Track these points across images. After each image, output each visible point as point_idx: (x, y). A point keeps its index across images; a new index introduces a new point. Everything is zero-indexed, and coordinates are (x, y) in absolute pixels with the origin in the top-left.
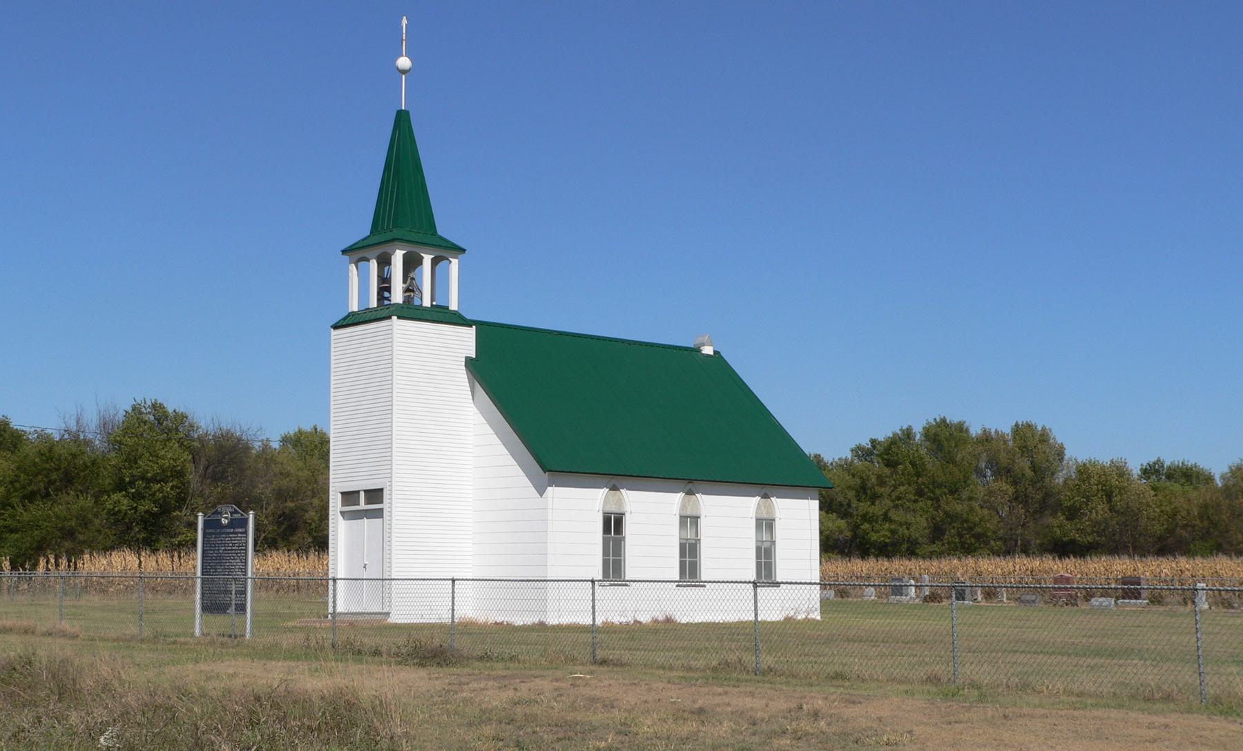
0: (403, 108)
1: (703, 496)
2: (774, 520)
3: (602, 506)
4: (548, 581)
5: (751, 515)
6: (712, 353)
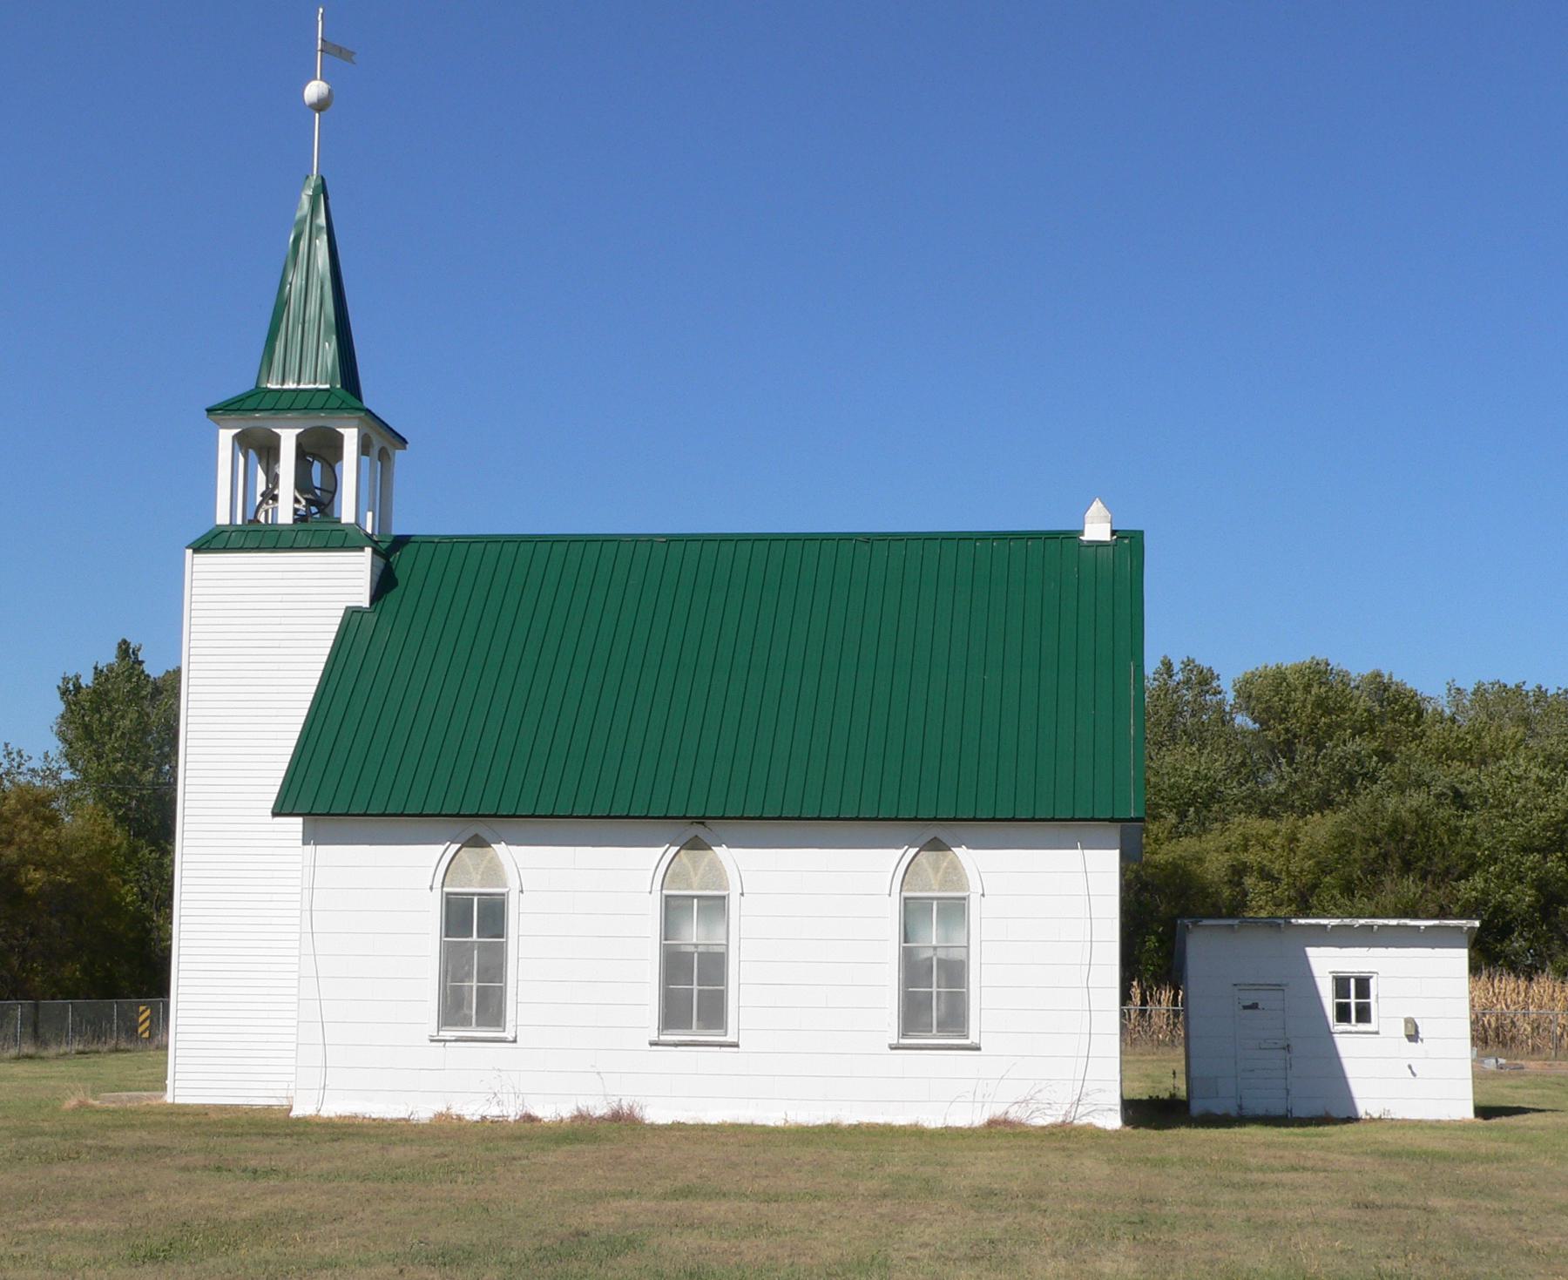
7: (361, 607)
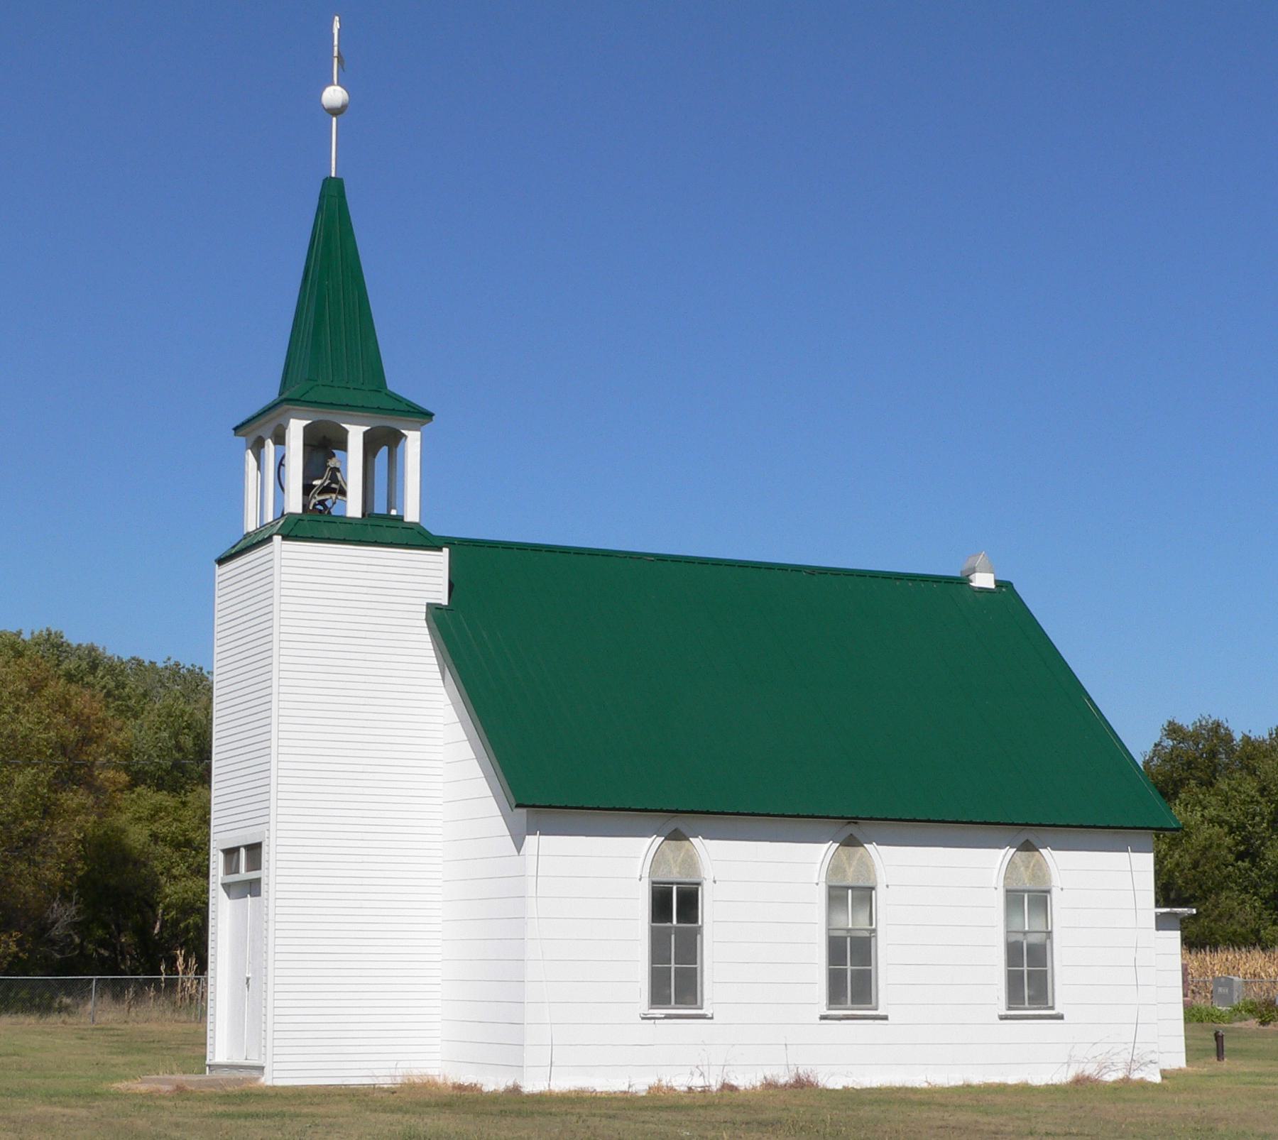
0: (333, 175)
1: (879, 847)
2: (1048, 891)
3: (647, 870)
5: (994, 884)
6: (992, 586)
7: (440, 604)
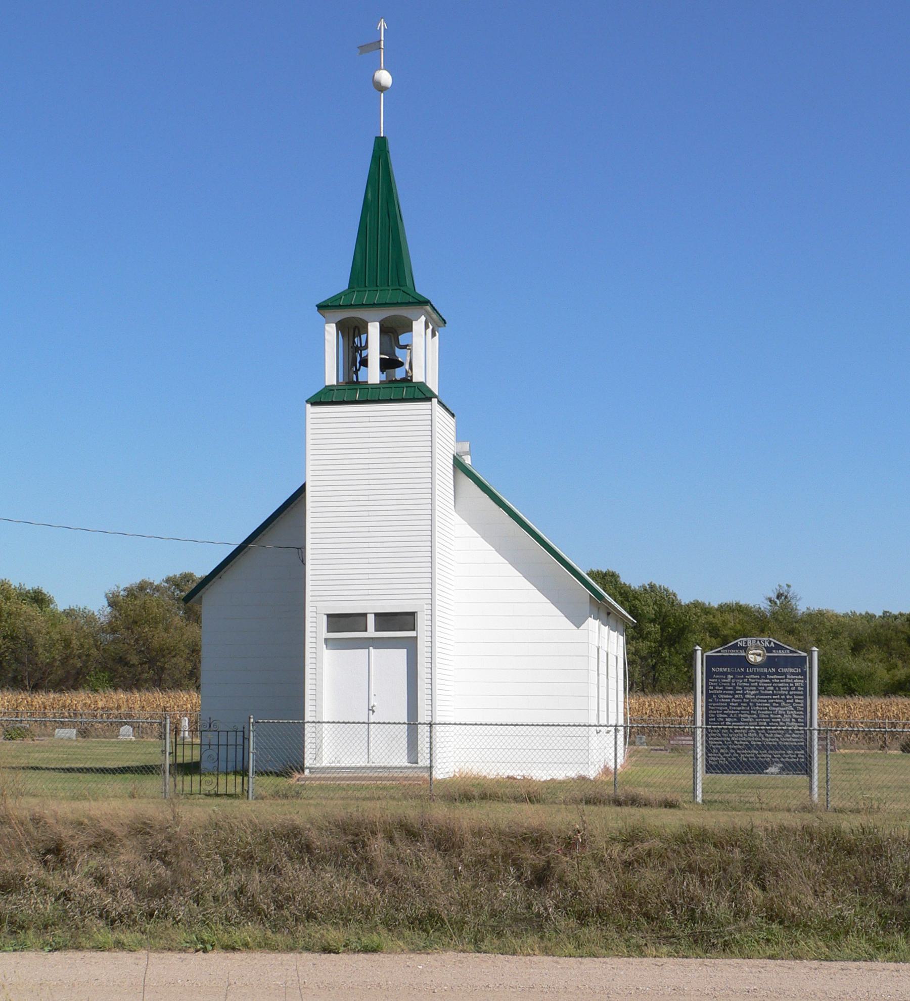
4: (324, 722)
